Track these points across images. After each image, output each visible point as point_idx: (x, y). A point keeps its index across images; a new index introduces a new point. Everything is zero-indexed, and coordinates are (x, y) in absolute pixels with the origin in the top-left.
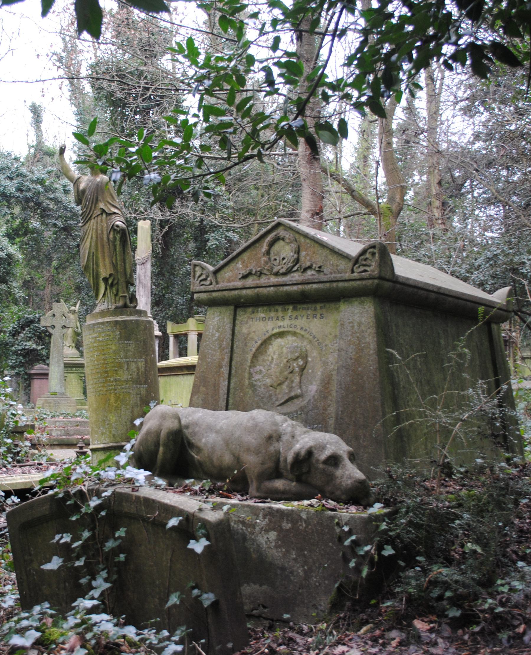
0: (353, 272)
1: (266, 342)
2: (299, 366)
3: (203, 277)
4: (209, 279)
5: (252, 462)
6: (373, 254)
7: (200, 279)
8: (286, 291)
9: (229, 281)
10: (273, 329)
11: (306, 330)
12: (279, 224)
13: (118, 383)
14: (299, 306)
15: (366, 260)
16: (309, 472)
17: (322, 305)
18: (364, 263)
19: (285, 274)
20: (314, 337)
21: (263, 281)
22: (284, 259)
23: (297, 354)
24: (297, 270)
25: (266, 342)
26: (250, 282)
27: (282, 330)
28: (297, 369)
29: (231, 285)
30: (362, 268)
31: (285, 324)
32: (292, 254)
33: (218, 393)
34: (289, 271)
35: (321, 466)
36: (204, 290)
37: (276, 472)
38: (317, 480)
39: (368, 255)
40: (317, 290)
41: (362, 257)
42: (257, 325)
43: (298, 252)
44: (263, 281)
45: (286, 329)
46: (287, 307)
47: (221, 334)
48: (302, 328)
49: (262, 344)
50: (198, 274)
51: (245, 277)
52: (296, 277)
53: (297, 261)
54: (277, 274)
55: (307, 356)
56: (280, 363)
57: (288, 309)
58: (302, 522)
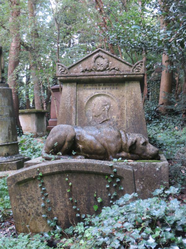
0: (133, 71)
1: (92, 98)
2: (107, 108)
3: (63, 70)
4: (65, 71)
5: (113, 146)
6: (142, 65)
7: (61, 71)
8: (103, 78)
9: (75, 73)
10: (95, 93)
11: (110, 94)
12: (99, 50)
13: (180, 105)
14: (106, 84)
15: (139, 67)
16: (135, 149)
17: (117, 84)
18: (137, 68)
19: (102, 71)
20: (114, 97)
21: (92, 73)
22: (102, 64)
23: (107, 103)
24: (108, 69)
25: (92, 98)
26: (86, 73)
27: (99, 93)
28: (107, 109)
29: (77, 74)
30: (137, 70)
31: (101, 91)
32: (106, 63)
33: (71, 119)
34: (105, 70)
35: (141, 146)
36: (63, 76)
37: (121, 150)
38: (139, 151)
39: (139, 65)
40: (97, 78)
41: (137, 66)
42: (87, 93)
43: (108, 62)
44: (92, 73)
45: (101, 93)
46: (100, 84)
47: (71, 95)
48: (108, 93)
49: (90, 99)
50: (60, 69)
51: (83, 71)
52: (107, 72)
53: (108, 66)
54: (99, 71)
55: (110, 104)
56: (99, 107)
57: (101, 85)
58: (141, 168)
